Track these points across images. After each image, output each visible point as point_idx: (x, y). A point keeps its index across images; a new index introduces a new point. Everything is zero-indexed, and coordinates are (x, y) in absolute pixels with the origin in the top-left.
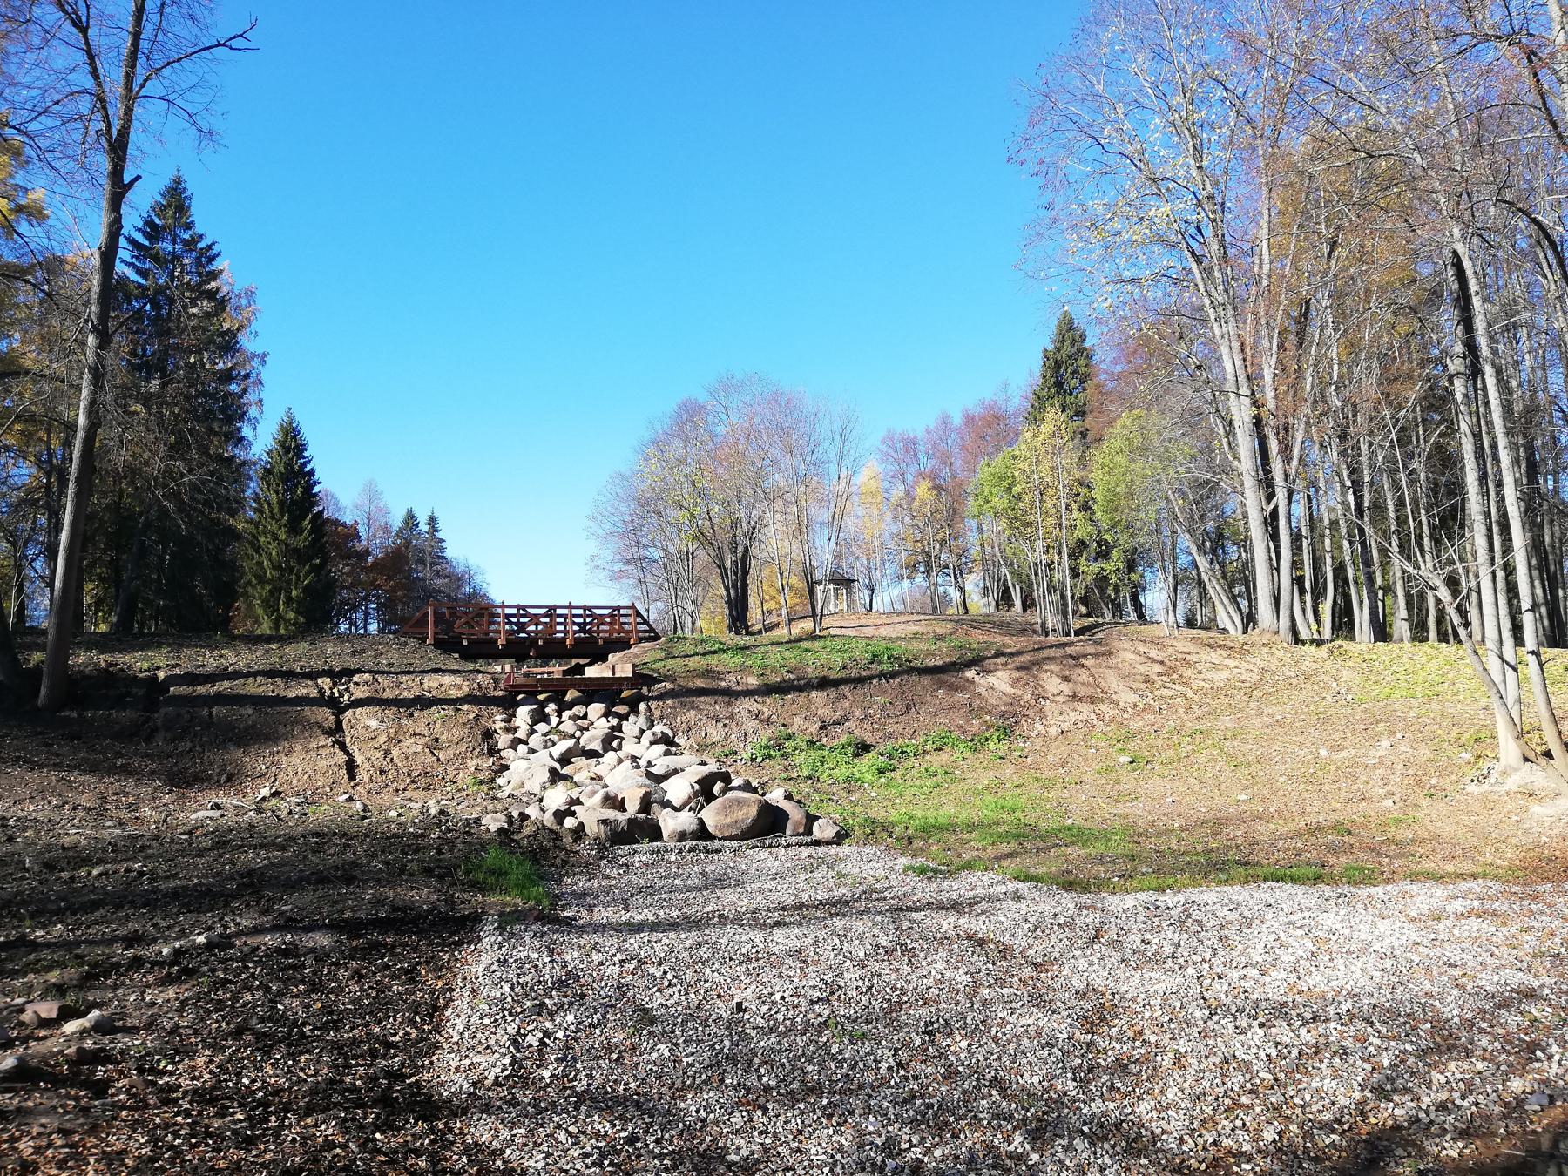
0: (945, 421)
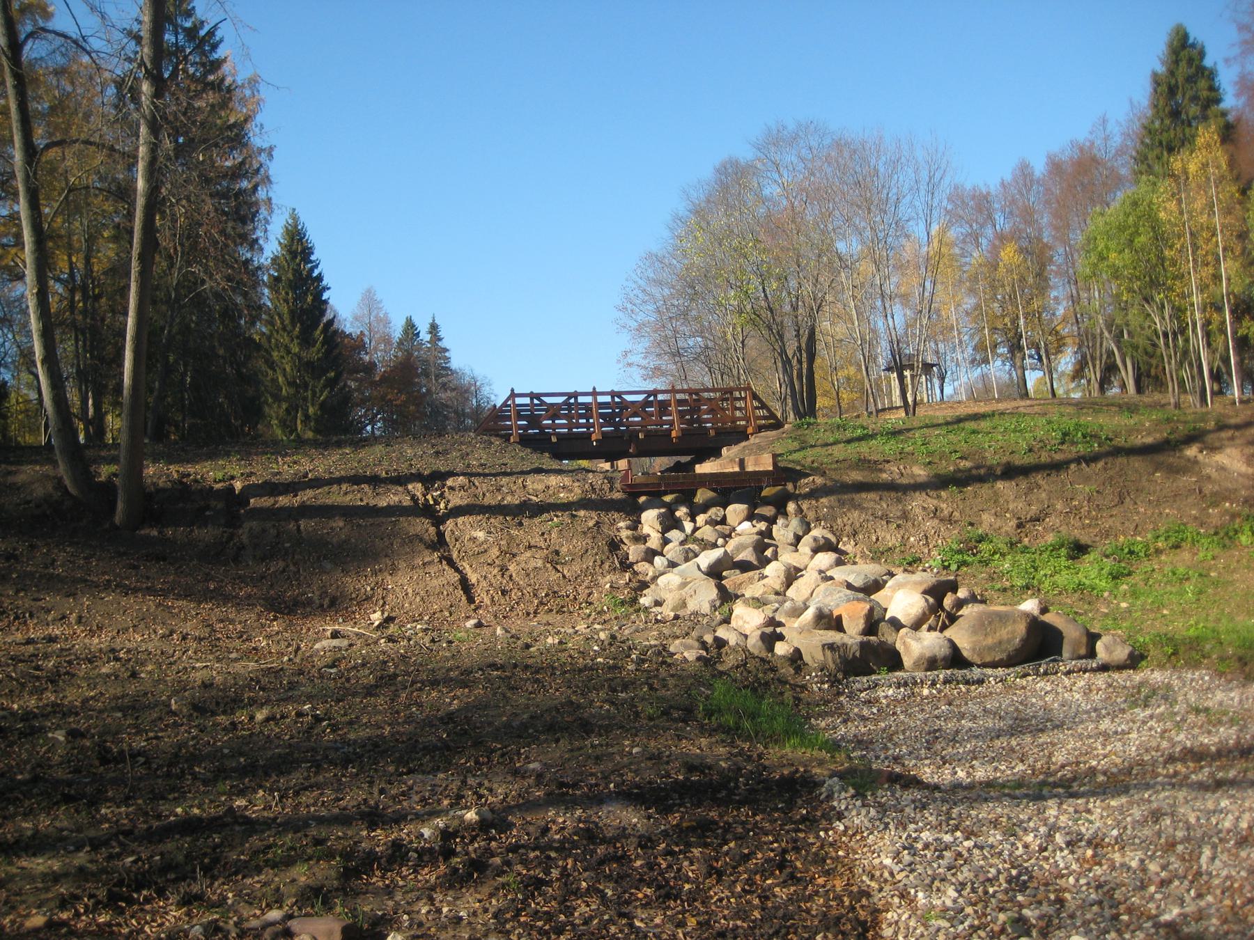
0: (1024, 171)
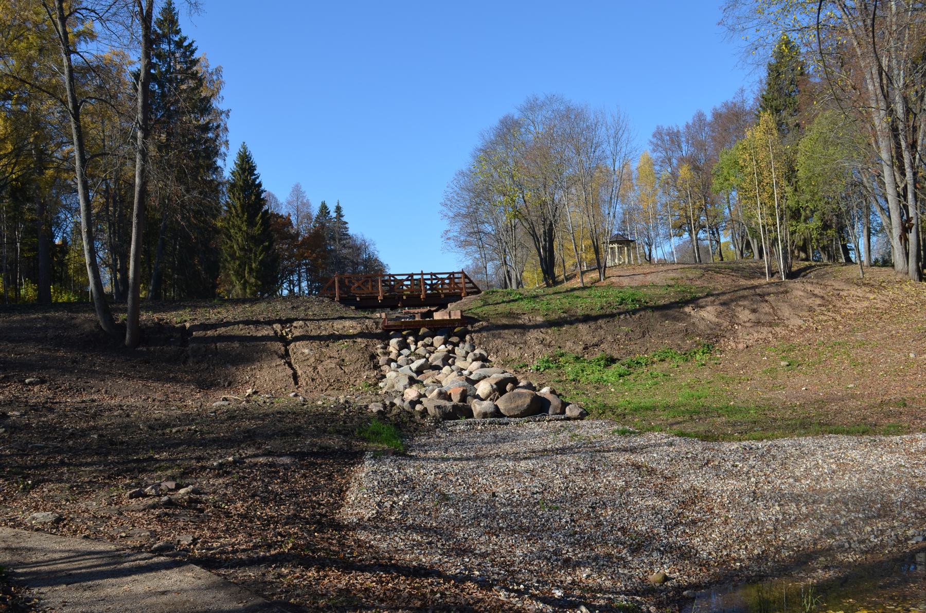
0: (700, 117)
